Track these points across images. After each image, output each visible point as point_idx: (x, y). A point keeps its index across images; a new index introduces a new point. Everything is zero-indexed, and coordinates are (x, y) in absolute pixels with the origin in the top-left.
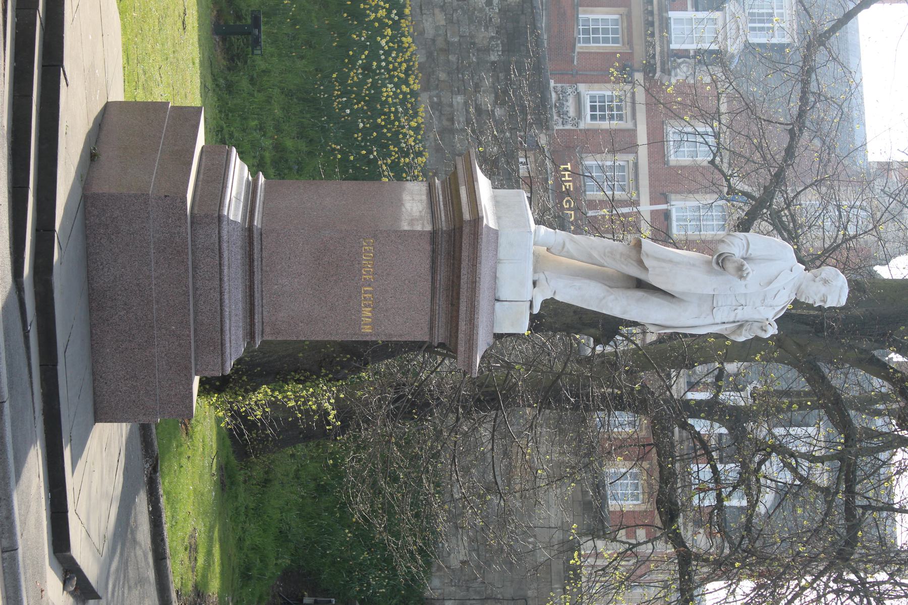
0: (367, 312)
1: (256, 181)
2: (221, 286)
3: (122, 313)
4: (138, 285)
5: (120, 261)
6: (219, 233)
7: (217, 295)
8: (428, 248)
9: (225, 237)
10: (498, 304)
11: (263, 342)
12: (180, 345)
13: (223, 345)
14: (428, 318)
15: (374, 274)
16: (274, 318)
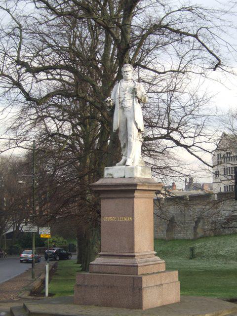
8: (106, 200)
14: (127, 199)
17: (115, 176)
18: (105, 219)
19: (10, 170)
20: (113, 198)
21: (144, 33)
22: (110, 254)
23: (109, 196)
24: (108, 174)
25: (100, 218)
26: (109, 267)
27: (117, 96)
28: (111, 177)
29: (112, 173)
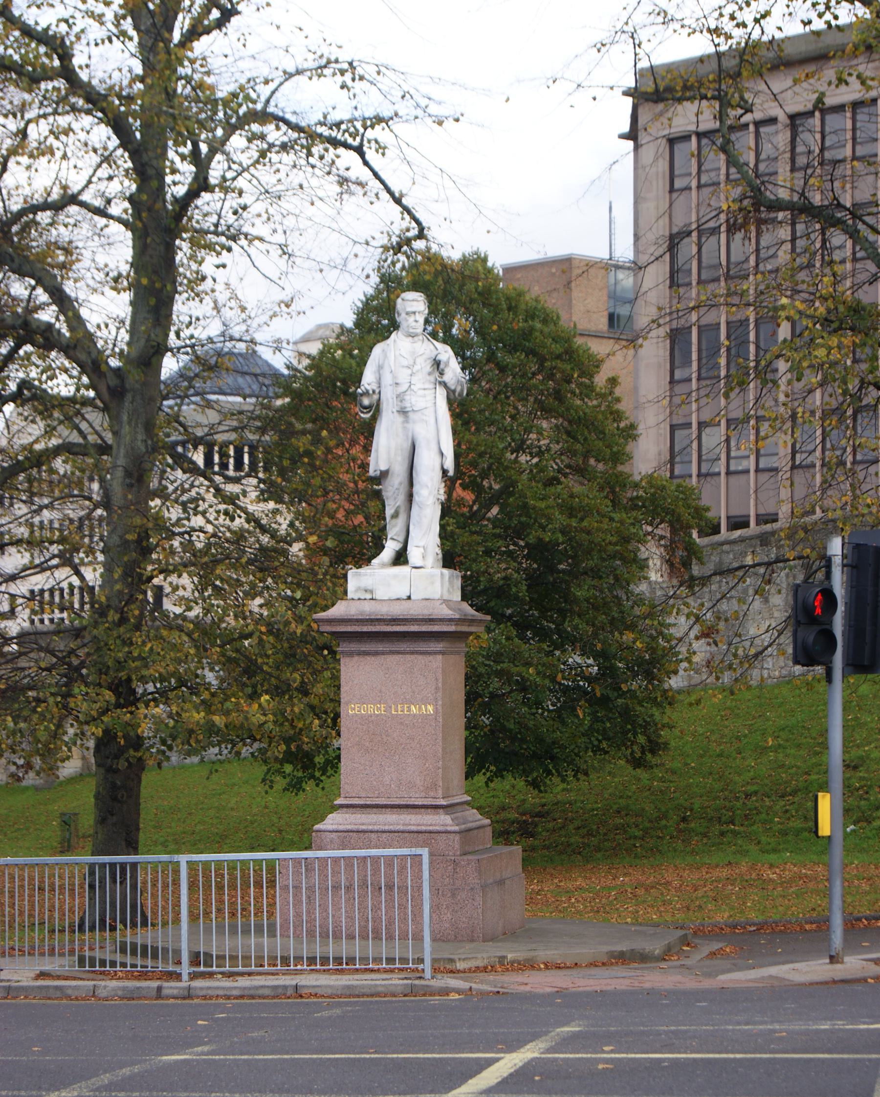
1: (342, 806)
7: (384, 835)
8: (356, 658)
9: (334, 827)
14: (420, 657)
17: (379, 595)
18: (352, 710)
19: (305, 556)
20: (376, 654)
21: (81, 102)
24: (358, 589)
25: (466, 674)
26: (373, 835)
27: (387, 379)
28: (369, 596)
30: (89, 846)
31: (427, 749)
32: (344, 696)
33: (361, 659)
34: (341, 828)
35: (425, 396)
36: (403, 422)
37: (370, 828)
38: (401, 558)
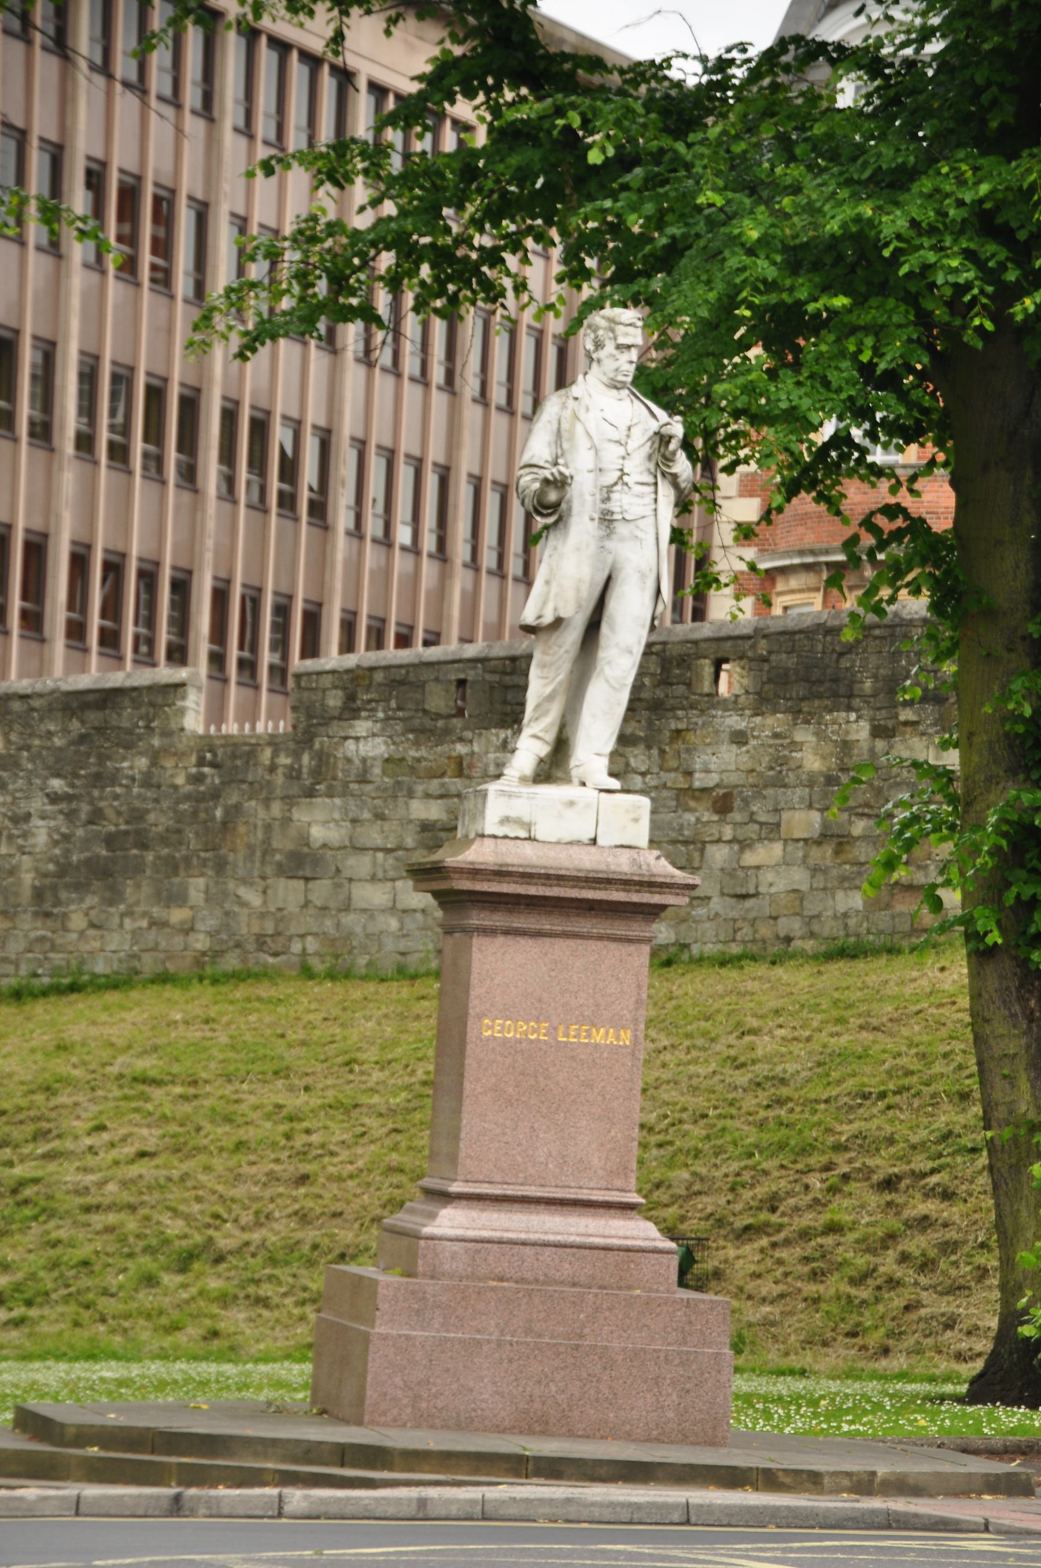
0: (599, 1037)
2: (534, 1244)
3: (554, 1388)
4: (510, 1361)
5: (471, 1384)
6: (451, 1240)
7: (548, 1251)
8: (501, 939)
9: (459, 1232)
10: (600, 841)
11: (639, 1191)
12: (609, 1309)
13: (628, 1250)
14: (613, 946)
15: (538, 1021)
16: (601, 1173)
17: (540, 833)
22: (560, 1194)
23: (520, 922)
24: (505, 820)
26: (528, 1250)
28: (523, 834)
29: (526, 819)
30: (398, 1270)
31: (615, 1104)
32: (475, 1005)
33: (510, 940)
34: (471, 1234)
35: (641, 496)
36: (602, 538)
37: (523, 1236)
38: (554, 767)
